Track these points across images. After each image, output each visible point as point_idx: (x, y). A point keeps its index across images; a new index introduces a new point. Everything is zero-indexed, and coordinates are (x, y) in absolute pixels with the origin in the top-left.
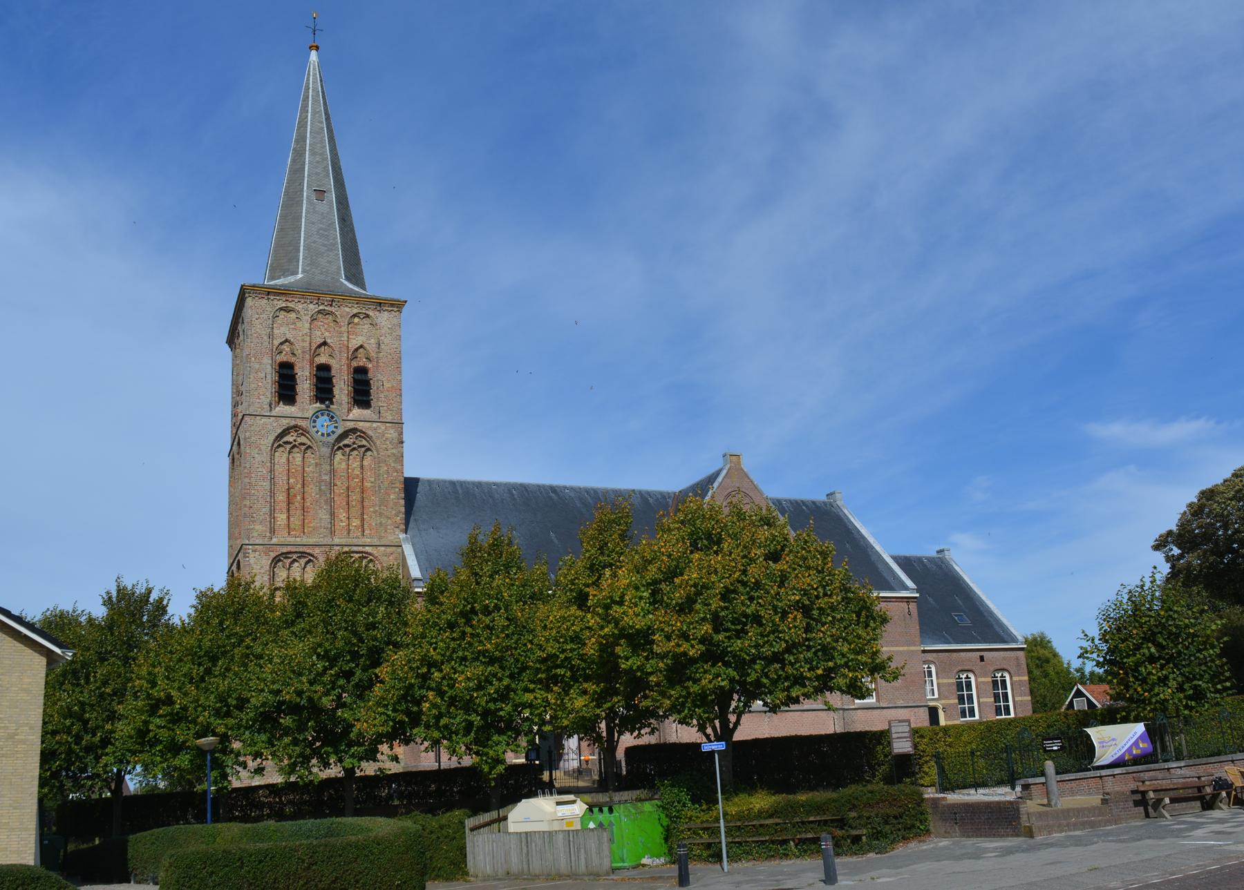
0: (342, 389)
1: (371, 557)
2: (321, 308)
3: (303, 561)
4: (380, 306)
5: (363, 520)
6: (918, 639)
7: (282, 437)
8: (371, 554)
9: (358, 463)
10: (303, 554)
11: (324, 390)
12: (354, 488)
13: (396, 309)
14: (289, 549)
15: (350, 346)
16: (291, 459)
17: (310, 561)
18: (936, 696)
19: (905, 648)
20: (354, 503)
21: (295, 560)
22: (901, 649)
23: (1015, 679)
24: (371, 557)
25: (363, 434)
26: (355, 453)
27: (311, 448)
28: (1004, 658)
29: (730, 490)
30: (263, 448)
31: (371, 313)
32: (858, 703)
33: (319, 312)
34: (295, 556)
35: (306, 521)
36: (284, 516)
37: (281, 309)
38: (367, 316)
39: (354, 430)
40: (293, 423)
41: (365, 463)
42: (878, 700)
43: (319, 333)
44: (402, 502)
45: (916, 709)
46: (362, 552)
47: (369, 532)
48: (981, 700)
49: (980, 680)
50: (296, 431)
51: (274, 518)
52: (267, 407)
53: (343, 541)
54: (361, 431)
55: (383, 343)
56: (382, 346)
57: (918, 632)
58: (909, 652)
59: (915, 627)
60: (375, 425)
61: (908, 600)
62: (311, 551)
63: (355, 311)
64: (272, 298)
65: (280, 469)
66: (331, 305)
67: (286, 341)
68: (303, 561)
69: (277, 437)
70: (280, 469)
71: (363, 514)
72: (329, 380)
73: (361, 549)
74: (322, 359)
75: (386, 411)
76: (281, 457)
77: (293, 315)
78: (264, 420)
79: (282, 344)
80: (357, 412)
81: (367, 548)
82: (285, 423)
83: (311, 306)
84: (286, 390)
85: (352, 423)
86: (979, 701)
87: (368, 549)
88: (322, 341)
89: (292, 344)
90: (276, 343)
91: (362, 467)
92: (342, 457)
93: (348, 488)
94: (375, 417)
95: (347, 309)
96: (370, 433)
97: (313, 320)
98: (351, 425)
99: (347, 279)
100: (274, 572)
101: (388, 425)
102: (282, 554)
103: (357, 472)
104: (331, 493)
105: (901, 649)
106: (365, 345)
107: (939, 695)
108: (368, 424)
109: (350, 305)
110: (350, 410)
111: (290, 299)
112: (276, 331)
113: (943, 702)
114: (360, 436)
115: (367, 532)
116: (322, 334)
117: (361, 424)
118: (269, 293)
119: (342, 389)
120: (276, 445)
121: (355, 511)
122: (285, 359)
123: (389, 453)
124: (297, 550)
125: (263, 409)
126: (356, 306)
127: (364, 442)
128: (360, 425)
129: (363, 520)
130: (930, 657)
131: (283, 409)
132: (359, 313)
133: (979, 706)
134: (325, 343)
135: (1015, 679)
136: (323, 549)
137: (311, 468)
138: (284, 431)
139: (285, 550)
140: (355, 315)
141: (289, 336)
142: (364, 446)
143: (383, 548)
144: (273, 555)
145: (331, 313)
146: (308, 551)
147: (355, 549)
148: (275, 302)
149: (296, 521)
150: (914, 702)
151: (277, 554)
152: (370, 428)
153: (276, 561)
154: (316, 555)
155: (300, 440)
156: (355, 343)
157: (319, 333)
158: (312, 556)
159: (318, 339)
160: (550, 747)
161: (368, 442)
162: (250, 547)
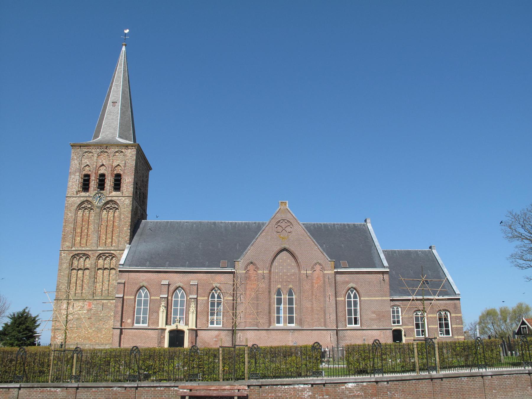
0: (109, 183)
1: (114, 255)
2: (102, 150)
3: (84, 257)
4: (127, 147)
5: (112, 239)
6: (388, 293)
7: (81, 205)
8: (113, 254)
9: (113, 215)
10: (84, 255)
11: (101, 185)
12: (110, 226)
13: (134, 148)
14: (79, 252)
15: (113, 165)
16: (84, 214)
17: (87, 257)
18: (401, 324)
19: (380, 298)
20: (109, 232)
21: (107, 257)
22: (377, 298)
23: (452, 315)
24: (114, 255)
25: (115, 202)
26: (111, 211)
27: (93, 209)
28: (446, 304)
29: (279, 220)
30: (72, 210)
31: (123, 150)
32: (136, 326)
33: (101, 152)
34: (107, 255)
35: (88, 241)
36: (79, 238)
37: (86, 152)
38: (122, 152)
39: (111, 201)
40: (85, 199)
41: (116, 215)
42: (148, 326)
43: (101, 161)
44: (129, 231)
45: (384, 331)
46: (110, 253)
47: (115, 244)
48: (429, 327)
49: (452, 315)
50: (112, 202)
51: (75, 239)
52: (75, 193)
53: (102, 248)
54: (114, 201)
55: (127, 163)
56: (127, 164)
57: (388, 290)
58: (382, 300)
59: (387, 287)
60: (120, 198)
61: (383, 273)
62: (87, 253)
63: (117, 150)
64: (82, 148)
65: (79, 219)
66: (106, 149)
67: (87, 165)
68: (84, 257)
69: (79, 205)
70: (79, 219)
71: (112, 237)
72: (88, 180)
73: (109, 252)
74: (102, 171)
75: (126, 192)
76: (80, 213)
77: (91, 154)
78: (74, 198)
79: (85, 166)
80: (114, 193)
81: (112, 251)
82: (82, 199)
83: (98, 150)
84: (85, 186)
85: (110, 198)
86: (428, 327)
87: (112, 252)
88: (101, 164)
89: (89, 166)
90: (83, 166)
91: (114, 216)
92: (106, 212)
93: (107, 226)
94: (121, 195)
95: (113, 150)
96: (118, 202)
97: (99, 156)
98: (109, 199)
99: (120, 137)
100: (72, 262)
101: (126, 198)
102: (76, 254)
103: (112, 219)
104: (99, 228)
105: (377, 298)
106: (120, 164)
107: (402, 323)
108: (117, 198)
109: (114, 148)
110: (110, 192)
111: (89, 148)
112: (83, 162)
113: (404, 327)
114: (114, 204)
115: (114, 244)
116: (102, 161)
117: (114, 198)
118: (80, 146)
119: (109, 183)
120: (78, 209)
121: (109, 236)
122: (86, 173)
123: (125, 210)
124: (82, 253)
125: (73, 194)
126: (117, 148)
127: (116, 206)
128: (114, 198)
129: (112, 239)
130: (397, 303)
131: (83, 194)
132: (118, 151)
133: (428, 330)
134: (103, 165)
135: (453, 315)
136: (92, 252)
137: (92, 218)
138: (81, 203)
139: (77, 253)
140: (117, 152)
141: (88, 163)
142: (115, 207)
143: (119, 251)
144: (71, 255)
145: (107, 152)
146: (86, 253)
147: (106, 252)
148: (83, 149)
149: (84, 241)
150: (383, 327)
151: (74, 254)
152: (118, 199)
153: (74, 257)
154: (89, 255)
155: (113, 206)
156: (115, 164)
157: (101, 161)
158: (88, 255)
159: (100, 164)
160: (62, 343)
161: (117, 205)
162: (63, 252)
